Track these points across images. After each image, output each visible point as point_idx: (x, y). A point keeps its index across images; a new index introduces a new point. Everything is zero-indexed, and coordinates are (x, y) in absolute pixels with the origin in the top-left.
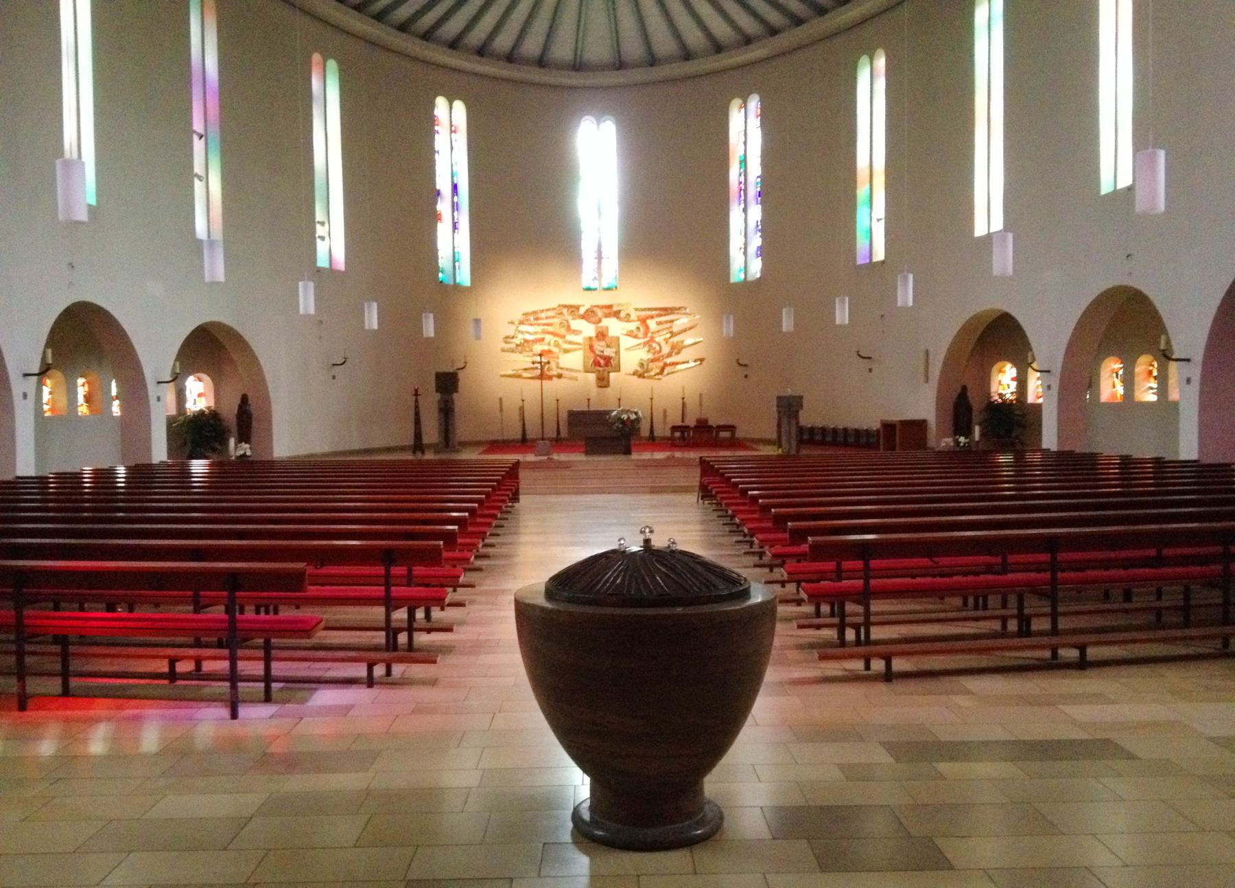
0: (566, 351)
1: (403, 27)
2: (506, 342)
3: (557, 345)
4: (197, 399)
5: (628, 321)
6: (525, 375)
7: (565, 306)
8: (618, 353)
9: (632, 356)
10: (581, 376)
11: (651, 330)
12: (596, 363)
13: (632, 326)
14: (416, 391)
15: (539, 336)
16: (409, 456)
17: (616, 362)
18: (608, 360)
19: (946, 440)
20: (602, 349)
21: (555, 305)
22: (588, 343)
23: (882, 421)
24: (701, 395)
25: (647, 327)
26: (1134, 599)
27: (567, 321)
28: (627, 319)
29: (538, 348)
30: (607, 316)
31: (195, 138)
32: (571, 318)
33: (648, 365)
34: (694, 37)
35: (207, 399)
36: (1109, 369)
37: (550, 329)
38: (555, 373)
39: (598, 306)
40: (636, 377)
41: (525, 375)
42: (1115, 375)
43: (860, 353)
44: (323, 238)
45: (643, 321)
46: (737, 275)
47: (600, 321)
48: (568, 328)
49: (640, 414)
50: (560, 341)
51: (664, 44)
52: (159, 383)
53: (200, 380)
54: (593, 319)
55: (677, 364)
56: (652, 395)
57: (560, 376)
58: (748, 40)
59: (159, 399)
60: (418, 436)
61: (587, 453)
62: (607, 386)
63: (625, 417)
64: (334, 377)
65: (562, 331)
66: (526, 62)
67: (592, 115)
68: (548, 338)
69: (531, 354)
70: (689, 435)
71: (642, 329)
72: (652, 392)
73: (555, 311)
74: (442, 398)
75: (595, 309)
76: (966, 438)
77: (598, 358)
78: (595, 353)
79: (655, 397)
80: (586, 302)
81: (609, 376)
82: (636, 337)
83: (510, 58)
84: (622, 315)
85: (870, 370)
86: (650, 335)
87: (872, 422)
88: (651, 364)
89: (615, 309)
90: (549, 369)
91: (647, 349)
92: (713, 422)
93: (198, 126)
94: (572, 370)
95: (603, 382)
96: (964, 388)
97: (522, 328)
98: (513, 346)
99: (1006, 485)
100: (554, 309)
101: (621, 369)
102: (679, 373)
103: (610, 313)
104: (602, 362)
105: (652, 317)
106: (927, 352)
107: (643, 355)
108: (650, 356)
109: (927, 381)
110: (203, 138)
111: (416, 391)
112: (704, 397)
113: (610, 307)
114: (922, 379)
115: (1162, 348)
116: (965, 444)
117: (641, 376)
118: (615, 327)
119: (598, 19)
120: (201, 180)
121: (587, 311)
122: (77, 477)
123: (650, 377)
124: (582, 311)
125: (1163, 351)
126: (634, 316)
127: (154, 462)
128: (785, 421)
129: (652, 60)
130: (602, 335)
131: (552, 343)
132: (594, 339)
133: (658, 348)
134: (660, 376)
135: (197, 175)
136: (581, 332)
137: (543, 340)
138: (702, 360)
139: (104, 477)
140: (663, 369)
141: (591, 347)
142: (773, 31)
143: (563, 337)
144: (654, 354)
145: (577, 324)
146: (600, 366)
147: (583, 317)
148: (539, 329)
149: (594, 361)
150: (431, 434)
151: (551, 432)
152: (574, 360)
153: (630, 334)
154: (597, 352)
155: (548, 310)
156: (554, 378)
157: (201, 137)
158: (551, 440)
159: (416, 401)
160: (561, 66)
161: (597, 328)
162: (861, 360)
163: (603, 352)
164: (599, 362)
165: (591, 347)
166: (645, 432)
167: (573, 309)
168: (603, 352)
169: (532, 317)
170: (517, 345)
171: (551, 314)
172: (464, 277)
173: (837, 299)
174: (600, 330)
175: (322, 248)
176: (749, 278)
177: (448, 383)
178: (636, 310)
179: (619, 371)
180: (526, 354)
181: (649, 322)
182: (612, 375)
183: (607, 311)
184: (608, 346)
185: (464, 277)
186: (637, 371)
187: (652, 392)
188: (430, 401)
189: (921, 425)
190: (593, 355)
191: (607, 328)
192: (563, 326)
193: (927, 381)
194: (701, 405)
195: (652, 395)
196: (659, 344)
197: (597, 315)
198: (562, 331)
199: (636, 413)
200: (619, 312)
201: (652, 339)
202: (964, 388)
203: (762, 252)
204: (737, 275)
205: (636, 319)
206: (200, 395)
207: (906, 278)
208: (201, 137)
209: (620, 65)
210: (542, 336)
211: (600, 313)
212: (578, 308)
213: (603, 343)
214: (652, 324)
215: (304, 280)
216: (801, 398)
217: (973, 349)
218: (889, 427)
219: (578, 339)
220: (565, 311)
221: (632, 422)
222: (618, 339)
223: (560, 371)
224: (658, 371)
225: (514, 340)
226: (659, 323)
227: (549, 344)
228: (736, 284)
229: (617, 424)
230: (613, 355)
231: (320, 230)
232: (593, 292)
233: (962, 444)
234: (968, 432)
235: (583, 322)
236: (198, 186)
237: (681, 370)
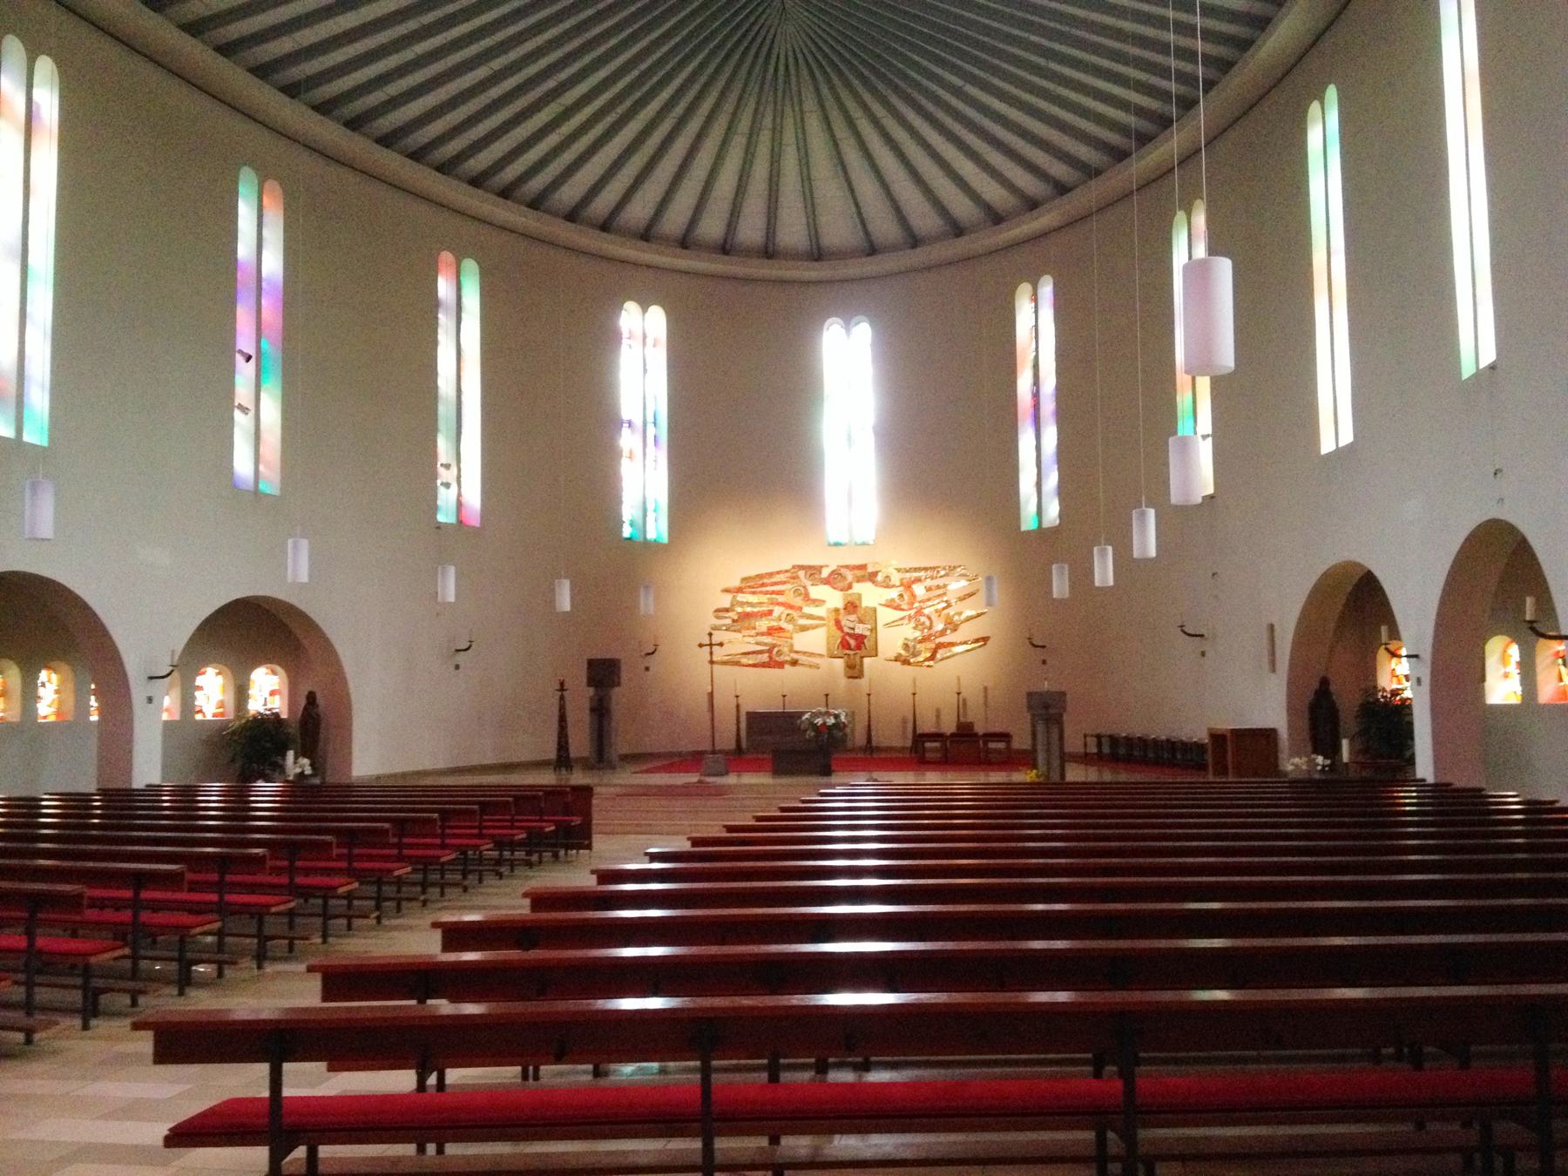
0: (804, 629)
1: (572, 216)
2: (717, 617)
3: (790, 619)
4: (269, 699)
5: (888, 587)
6: (744, 661)
7: (801, 567)
8: (874, 630)
9: (893, 635)
10: (825, 663)
11: (919, 599)
12: (845, 645)
13: (893, 594)
14: (562, 684)
15: (765, 608)
16: (547, 778)
17: (872, 643)
18: (860, 639)
19: (1297, 760)
20: (852, 625)
21: (788, 567)
22: (833, 616)
23: (1209, 729)
24: (986, 689)
25: (913, 596)
26: (1427, 1065)
27: (804, 587)
28: (887, 584)
29: (763, 625)
30: (859, 580)
31: (239, 359)
32: (810, 583)
33: (915, 648)
34: (962, 208)
35: (281, 698)
36: (1552, 651)
37: (781, 599)
38: (788, 658)
39: (847, 567)
40: (899, 663)
41: (744, 661)
42: (1560, 661)
43: (1186, 629)
44: (447, 485)
45: (908, 586)
46: (1029, 522)
47: (850, 587)
48: (806, 597)
49: (843, 718)
50: (795, 614)
51: (924, 219)
52: (151, 678)
53: (274, 673)
54: (841, 585)
55: (952, 644)
56: (959, 688)
57: (794, 663)
58: (1032, 204)
59: (150, 700)
60: (563, 745)
61: (777, 772)
62: (860, 675)
63: (819, 721)
64: (457, 667)
65: (798, 601)
66: (747, 253)
67: (838, 316)
68: (778, 610)
69: (753, 633)
70: (936, 750)
71: (906, 597)
72: (959, 684)
73: (788, 575)
74: (595, 695)
75: (843, 571)
76: (1326, 757)
77: (847, 638)
78: (842, 631)
79: (963, 690)
80: (830, 562)
81: (862, 662)
82: (898, 608)
83: (725, 248)
84: (880, 578)
85: (1203, 654)
86: (916, 605)
87: (1195, 729)
88: (918, 646)
89: (870, 569)
90: (779, 653)
91: (912, 624)
92: (980, 729)
93: (245, 342)
94: (811, 654)
95: (854, 671)
96: (1325, 682)
97: (741, 597)
98: (728, 621)
99: (1411, 829)
100: (787, 571)
101: (879, 654)
102: (955, 658)
103: (863, 576)
104: (852, 642)
105: (918, 580)
106: (1271, 628)
107: (909, 632)
108: (918, 634)
109: (1273, 669)
110: (253, 361)
111: (562, 684)
112: (989, 692)
113: (863, 567)
114: (1266, 666)
115: (1528, 617)
116: (1324, 766)
117: (906, 662)
118: (870, 595)
119: (829, 191)
120: (633, 431)
121: (833, 573)
122: (30, 806)
123: (919, 664)
124: (825, 573)
125: (1531, 622)
126: (896, 578)
127: (135, 786)
128: (1040, 728)
129: (914, 241)
130: (852, 606)
131: (784, 616)
132: (842, 611)
133: (928, 623)
134: (931, 663)
135: (240, 407)
136: (824, 601)
137: (770, 612)
138: (985, 639)
139: (75, 804)
140: (934, 652)
141: (838, 623)
142: (1062, 189)
143: (800, 609)
144: (922, 631)
145: (817, 591)
146: (850, 648)
147: (827, 582)
148: (764, 598)
149: (841, 642)
150: (580, 744)
151: (726, 740)
152: (815, 641)
153: (891, 605)
154: (846, 630)
155: (778, 573)
156: (787, 666)
157: (249, 358)
158: (726, 753)
159: (562, 698)
160: (794, 256)
161: (846, 596)
162: (1187, 637)
163: (853, 629)
164: (848, 644)
165: (838, 623)
166: (859, 739)
167: (813, 571)
168: (853, 629)
169: (754, 583)
170: (734, 621)
171: (782, 577)
172: (658, 529)
173: (1095, 549)
174: (849, 599)
175: (446, 499)
176: (1046, 525)
177: (603, 674)
178: (899, 570)
179: (876, 655)
180: (746, 632)
181: (914, 587)
182: (867, 661)
183: (859, 573)
184: (861, 621)
185: (658, 529)
186: (900, 655)
187: (959, 684)
188: (581, 697)
189: (1269, 735)
190: (839, 634)
191: (860, 596)
192: (800, 595)
193: (1273, 669)
194: (986, 704)
195: (959, 688)
196: (929, 618)
197: (844, 578)
198: (798, 601)
199: (837, 717)
200: (875, 574)
201: (919, 612)
202: (1325, 682)
203: (1063, 492)
204: (1029, 522)
205: (898, 584)
206: (273, 693)
207: (1143, 515)
208: (249, 358)
209: (872, 249)
210: (771, 608)
211: (850, 576)
212: (819, 569)
213: (853, 617)
214: (919, 590)
215: (1100, 544)
216: (1063, 694)
217: (1342, 617)
218: (1218, 738)
219: (820, 611)
220: (801, 574)
221: (830, 728)
222: (875, 610)
223: (795, 656)
224: (928, 655)
225: (730, 614)
226: (929, 589)
227: (779, 619)
228: (1028, 533)
229: (808, 732)
230: (867, 633)
231: (445, 475)
232: (841, 547)
233: (1319, 768)
234: (1332, 751)
235: (827, 588)
236: (242, 422)
237: (957, 654)
